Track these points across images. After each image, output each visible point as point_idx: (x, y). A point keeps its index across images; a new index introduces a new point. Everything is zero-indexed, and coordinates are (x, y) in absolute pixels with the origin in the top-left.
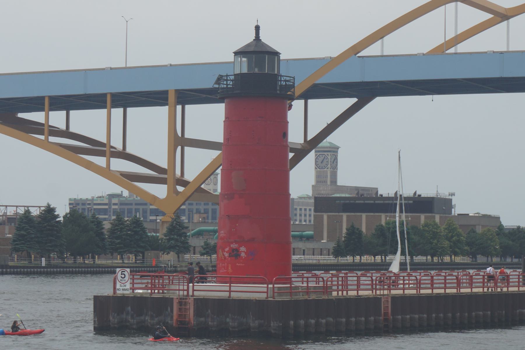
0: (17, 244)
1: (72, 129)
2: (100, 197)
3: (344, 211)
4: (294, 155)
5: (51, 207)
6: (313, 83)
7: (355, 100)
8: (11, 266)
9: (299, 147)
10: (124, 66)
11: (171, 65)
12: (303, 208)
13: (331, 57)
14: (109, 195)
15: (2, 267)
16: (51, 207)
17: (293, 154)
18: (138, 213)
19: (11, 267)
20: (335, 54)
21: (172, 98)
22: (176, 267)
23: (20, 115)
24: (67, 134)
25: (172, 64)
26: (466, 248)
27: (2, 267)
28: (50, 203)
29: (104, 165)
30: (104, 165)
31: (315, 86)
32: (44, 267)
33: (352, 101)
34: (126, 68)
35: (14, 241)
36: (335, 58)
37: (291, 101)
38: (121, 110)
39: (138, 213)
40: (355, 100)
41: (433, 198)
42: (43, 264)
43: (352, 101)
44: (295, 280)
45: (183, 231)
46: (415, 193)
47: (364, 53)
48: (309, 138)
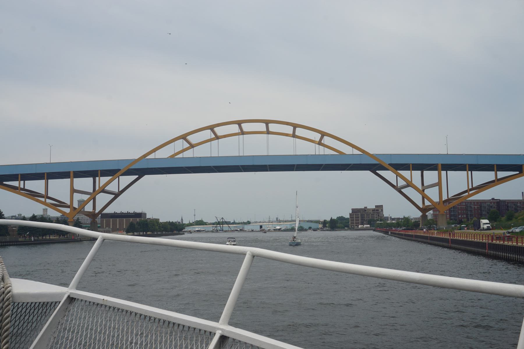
0: (20, 232)
1: (26, 188)
2: (9, 217)
3: (111, 218)
4: (114, 197)
5: (35, 215)
6: (127, 169)
7: (138, 176)
8: (20, 241)
9: (117, 193)
10: (49, 162)
11: (71, 162)
12: (84, 219)
13: (135, 159)
14: (12, 216)
15: (1, 242)
16: (35, 215)
17: (114, 196)
18: (518, 172)
19: (20, 242)
20: (137, 158)
21: (72, 175)
22: (80, 239)
23: (4, 183)
24: (24, 189)
25: (72, 161)
26: (162, 229)
27: (1, 242)
28: (34, 214)
29: (44, 201)
30: (44, 201)
31: (129, 170)
32: (33, 241)
33: (136, 177)
34: (50, 163)
35: (19, 230)
36: (137, 159)
37: (110, 178)
38: (23, 182)
39: (518, 172)
40: (138, 176)
41: (141, 213)
42: (33, 240)
43: (136, 177)
44: (433, 234)
45: (81, 225)
46: (121, 212)
47: (147, 158)
48: (120, 190)
